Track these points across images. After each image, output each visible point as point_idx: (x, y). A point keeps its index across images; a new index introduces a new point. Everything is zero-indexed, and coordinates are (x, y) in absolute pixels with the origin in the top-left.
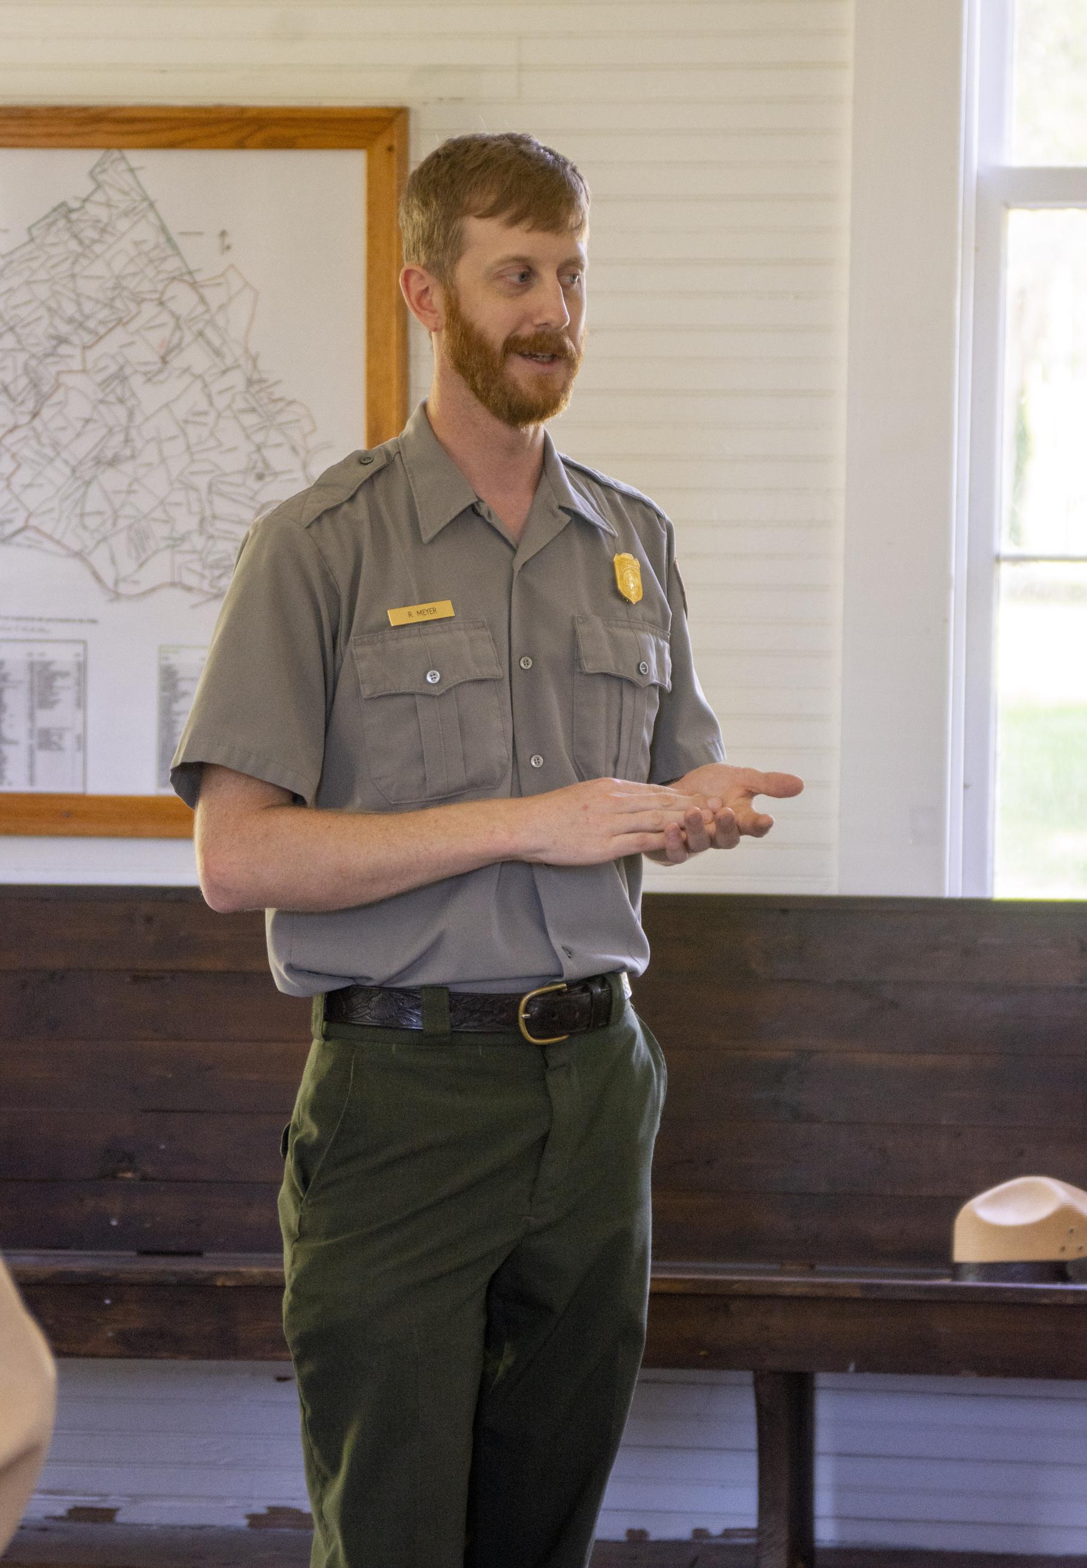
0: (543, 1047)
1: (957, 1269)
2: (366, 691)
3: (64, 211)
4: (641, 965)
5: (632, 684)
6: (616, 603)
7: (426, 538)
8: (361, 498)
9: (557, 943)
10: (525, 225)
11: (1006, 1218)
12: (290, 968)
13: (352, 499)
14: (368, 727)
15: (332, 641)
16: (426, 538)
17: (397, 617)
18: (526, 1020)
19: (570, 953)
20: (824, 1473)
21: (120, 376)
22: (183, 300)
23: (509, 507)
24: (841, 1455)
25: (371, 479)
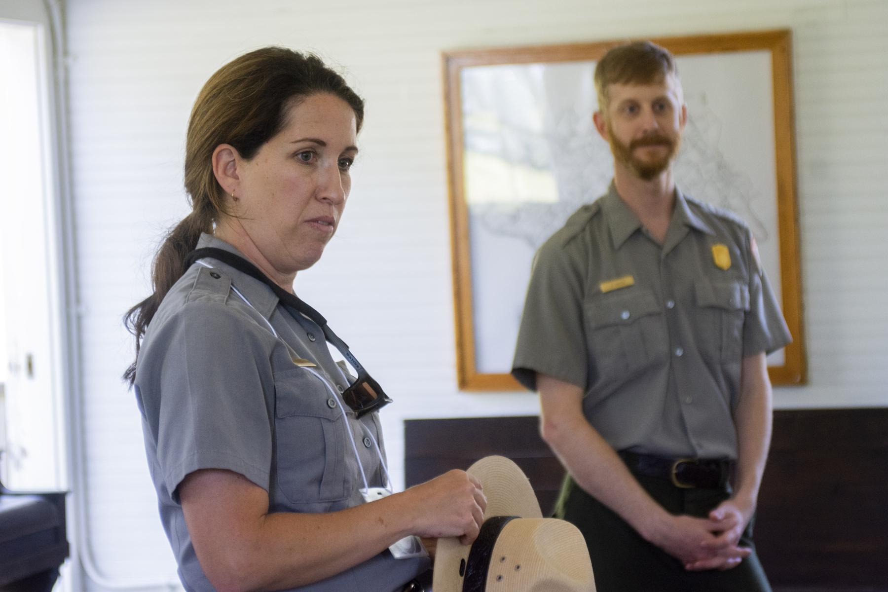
13: (583, 230)
17: (605, 287)
23: (657, 225)
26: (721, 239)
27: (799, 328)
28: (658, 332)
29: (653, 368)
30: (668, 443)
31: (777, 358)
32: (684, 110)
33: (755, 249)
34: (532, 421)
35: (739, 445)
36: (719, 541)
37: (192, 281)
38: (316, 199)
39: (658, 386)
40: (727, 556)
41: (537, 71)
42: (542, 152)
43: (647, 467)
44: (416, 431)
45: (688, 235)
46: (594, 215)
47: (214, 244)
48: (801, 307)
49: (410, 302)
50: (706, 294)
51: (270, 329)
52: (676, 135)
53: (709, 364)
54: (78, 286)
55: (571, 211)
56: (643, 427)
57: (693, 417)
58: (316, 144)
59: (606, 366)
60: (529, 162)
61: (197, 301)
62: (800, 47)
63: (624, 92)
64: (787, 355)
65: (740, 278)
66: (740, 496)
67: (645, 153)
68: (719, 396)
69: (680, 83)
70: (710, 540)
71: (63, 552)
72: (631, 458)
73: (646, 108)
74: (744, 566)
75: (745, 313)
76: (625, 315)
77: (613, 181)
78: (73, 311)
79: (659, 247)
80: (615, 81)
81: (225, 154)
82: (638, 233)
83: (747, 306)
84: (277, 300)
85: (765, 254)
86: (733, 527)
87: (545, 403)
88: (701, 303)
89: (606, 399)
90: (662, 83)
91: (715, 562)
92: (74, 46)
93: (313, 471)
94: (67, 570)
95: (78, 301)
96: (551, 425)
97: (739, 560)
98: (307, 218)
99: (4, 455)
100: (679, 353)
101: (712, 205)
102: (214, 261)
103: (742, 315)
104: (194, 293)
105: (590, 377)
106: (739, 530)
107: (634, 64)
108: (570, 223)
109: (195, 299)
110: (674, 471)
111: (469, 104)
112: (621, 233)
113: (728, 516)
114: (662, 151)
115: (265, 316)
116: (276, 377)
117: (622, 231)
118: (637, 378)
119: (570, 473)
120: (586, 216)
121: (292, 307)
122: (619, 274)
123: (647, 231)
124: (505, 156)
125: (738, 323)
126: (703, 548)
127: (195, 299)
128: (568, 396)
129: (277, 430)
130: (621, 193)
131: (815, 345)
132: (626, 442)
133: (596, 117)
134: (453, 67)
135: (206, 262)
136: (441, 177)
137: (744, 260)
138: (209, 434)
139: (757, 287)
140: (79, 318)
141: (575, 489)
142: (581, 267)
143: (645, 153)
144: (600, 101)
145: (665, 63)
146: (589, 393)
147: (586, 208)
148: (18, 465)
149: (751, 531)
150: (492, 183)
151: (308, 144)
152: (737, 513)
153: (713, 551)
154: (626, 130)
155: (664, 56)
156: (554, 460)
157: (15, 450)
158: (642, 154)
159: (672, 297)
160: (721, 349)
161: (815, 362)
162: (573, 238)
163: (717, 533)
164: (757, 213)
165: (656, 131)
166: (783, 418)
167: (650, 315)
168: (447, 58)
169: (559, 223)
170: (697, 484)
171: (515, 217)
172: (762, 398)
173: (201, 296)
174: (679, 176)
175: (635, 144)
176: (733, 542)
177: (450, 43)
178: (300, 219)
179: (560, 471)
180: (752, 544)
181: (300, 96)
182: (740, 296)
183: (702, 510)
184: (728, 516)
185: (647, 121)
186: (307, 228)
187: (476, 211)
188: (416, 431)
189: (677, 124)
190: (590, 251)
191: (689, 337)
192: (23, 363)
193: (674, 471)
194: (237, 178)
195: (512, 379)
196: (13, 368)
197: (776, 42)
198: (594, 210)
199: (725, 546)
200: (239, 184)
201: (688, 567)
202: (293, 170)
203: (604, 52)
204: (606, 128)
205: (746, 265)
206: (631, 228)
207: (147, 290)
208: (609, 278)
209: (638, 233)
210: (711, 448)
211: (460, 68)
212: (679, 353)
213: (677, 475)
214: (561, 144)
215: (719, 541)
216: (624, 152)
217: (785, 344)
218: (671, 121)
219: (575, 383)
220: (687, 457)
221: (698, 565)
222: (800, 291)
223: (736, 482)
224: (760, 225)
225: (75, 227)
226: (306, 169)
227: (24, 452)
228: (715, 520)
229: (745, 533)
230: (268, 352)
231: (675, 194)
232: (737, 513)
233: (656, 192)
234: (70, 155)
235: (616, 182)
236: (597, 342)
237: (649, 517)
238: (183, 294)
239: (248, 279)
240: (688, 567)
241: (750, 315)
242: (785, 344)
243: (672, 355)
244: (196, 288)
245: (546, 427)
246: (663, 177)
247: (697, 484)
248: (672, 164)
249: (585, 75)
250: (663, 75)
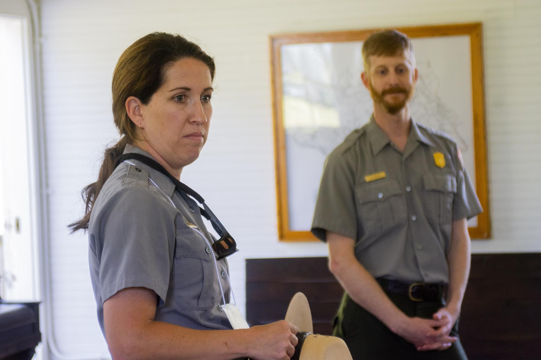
7: (375, 153)
13: (355, 144)
16: (375, 153)
17: (368, 178)
23: (400, 142)
26: (439, 149)
27: (487, 204)
28: (401, 206)
29: (398, 227)
30: (407, 274)
31: (473, 222)
32: (416, 71)
33: (460, 156)
34: (323, 261)
35: (450, 274)
36: (438, 333)
37: (125, 173)
38: (189, 122)
39: (400, 240)
40: (443, 342)
41: (327, 47)
43: (394, 289)
44: (253, 265)
45: (418, 147)
46: (361, 135)
47: (136, 151)
48: (488, 192)
49: (253, 188)
50: (430, 183)
51: (172, 204)
52: (410, 87)
53: (432, 224)
54: (47, 177)
55: (348, 133)
56: (391, 264)
57: (422, 258)
58: (183, 90)
59: (369, 227)
60: (322, 102)
61: (130, 185)
62: (488, 34)
63: (380, 61)
64: (479, 221)
65: (451, 173)
66: (451, 305)
67: (392, 98)
68: (438, 244)
69: (415, 55)
70: (432, 332)
71: (37, 338)
72: (386, 284)
73: (392, 70)
74: (453, 349)
75: (454, 194)
76: (381, 196)
77: (373, 115)
78: (44, 192)
79: (401, 154)
80: (374, 54)
82: (388, 145)
83: (455, 190)
84: (174, 187)
85: (466, 158)
86: (446, 324)
87: (332, 249)
88: (427, 188)
89: (369, 246)
90: (401, 55)
91: (435, 346)
93: (195, 291)
94: (40, 350)
95: (47, 186)
96: (335, 263)
97: (450, 344)
98: (185, 135)
99: (2, 279)
100: (414, 218)
101: (434, 128)
102: (136, 161)
103: (452, 195)
104: (128, 180)
105: (359, 234)
106: (450, 326)
107: (386, 44)
108: (347, 140)
109: (129, 183)
110: (410, 291)
111: (286, 67)
112: (378, 146)
113: (444, 318)
114: (401, 97)
115: (169, 196)
116: (177, 233)
117: (378, 144)
118: (388, 234)
119: (347, 292)
120: (357, 135)
121: (182, 190)
122: (376, 171)
123: (394, 145)
124: (308, 99)
125: (450, 200)
126: (428, 337)
127: (129, 183)
128: (346, 245)
129: (176, 265)
130: (378, 122)
131: (496, 215)
132: (383, 272)
133: (363, 76)
134: (276, 45)
135: (131, 162)
137: (454, 162)
138: (137, 265)
139: (461, 179)
140: (48, 196)
141: (350, 301)
142: (354, 168)
143: (392, 98)
144: (365, 66)
145: (404, 43)
146: (359, 243)
147: (357, 131)
148: (10, 286)
149: (457, 328)
150: (300, 115)
151: (179, 91)
152: (449, 316)
153: (434, 339)
154: (380, 84)
155: (403, 39)
156: (337, 284)
157: (9, 276)
158: (389, 98)
159: (409, 184)
160: (439, 216)
161: (496, 225)
162: (349, 149)
163: (436, 328)
164: (461, 134)
165: (397, 85)
166: (477, 259)
167: (396, 195)
168: (273, 39)
169: (340, 140)
170: (423, 299)
171: (313, 136)
172: (464, 246)
173: (132, 182)
174: (414, 111)
175: (385, 93)
176: (446, 333)
177: (275, 30)
178: (181, 136)
179: (340, 291)
180: (458, 335)
181: (171, 62)
182: (451, 184)
183: (429, 314)
184: (444, 318)
185: (392, 78)
186: (187, 140)
187: (290, 132)
188: (253, 265)
189: (411, 80)
190: (359, 156)
191: (420, 209)
192: (13, 223)
193: (410, 291)
195: (312, 235)
196: (7, 226)
197: (473, 30)
198: (361, 132)
199: (441, 336)
201: (419, 348)
202: (173, 108)
203: (368, 36)
204: (368, 82)
205: (454, 165)
206: (384, 143)
207: (94, 178)
208: (370, 173)
209: (388, 145)
210: (433, 276)
212: (414, 218)
213: (412, 293)
215: (438, 333)
216: (379, 97)
217: (478, 213)
218: (408, 79)
219: (349, 236)
220: (418, 282)
221: (425, 347)
222: (487, 181)
223: (448, 298)
224: (463, 142)
225: (45, 142)
226: (180, 106)
227: (14, 278)
228: (437, 319)
229: (453, 329)
230: (173, 218)
231: (411, 122)
232: (449, 316)
233: (399, 121)
234: (43, 97)
235: (375, 115)
236: (363, 212)
237: (395, 319)
238: (121, 180)
239: (157, 173)
240: (419, 348)
241: (457, 196)
242: (478, 213)
243: (409, 219)
244: (128, 177)
245: (332, 264)
246: (403, 112)
247: (423, 299)
248: (408, 104)
249: (356, 49)
250: (402, 51)
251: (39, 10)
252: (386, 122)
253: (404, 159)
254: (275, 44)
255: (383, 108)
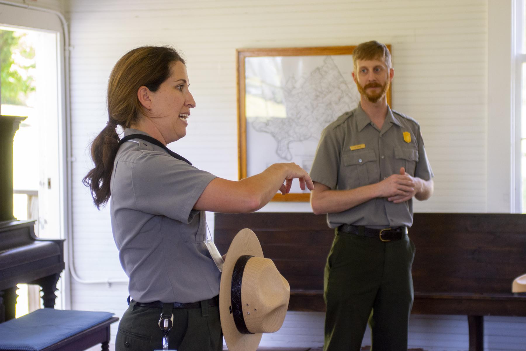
0: (385, 242)
1: (513, 294)
2: (346, 164)
3: (318, 69)
4: (410, 225)
5: (408, 161)
6: (404, 143)
7: (359, 130)
8: (346, 123)
9: (389, 218)
10: (364, 59)
11: (525, 282)
12: (330, 223)
13: (344, 122)
14: (346, 172)
15: (339, 154)
16: (359, 130)
17: (352, 148)
18: (381, 236)
19: (392, 220)
20: (486, 339)
21: (330, 104)
22: (343, 87)
23: (379, 122)
24: (490, 335)
25: (348, 118)
32: (392, 70)
41: (279, 59)
42: (280, 95)
46: (350, 116)
71: (62, 267)
73: (371, 70)
75: (416, 162)
77: (360, 102)
79: (379, 132)
81: (143, 92)
88: (397, 157)
92: (73, 42)
94: (63, 275)
103: (415, 163)
111: (248, 73)
120: (347, 116)
122: (359, 143)
124: (263, 96)
134: (241, 57)
136: (235, 105)
147: (347, 113)
148: (43, 227)
150: (257, 108)
157: (42, 220)
158: (369, 91)
168: (239, 52)
171: (267, 124)
177: (240, 46)
185: (371, 76)
187: (250, 121)
194: (150, 101)
200: (151, 103)
208: (354, 144)
211: (245, 58)
214: (289, 92)
216: (363, 89)
227: (46, 222)
251: (69, 26)
252: (369, 108)
253: (380, 135)
254: (241, 57)
255: (365, 98)
